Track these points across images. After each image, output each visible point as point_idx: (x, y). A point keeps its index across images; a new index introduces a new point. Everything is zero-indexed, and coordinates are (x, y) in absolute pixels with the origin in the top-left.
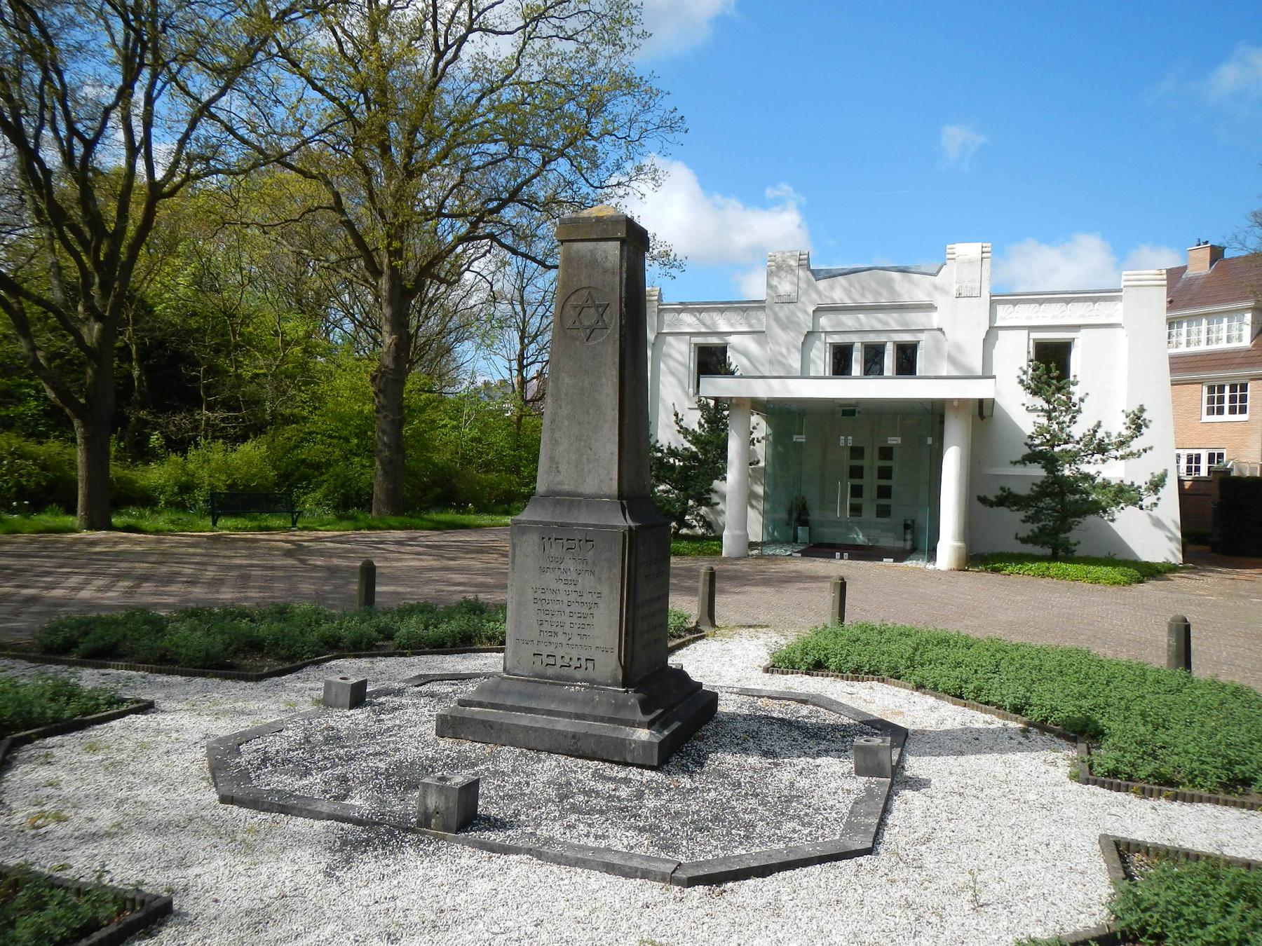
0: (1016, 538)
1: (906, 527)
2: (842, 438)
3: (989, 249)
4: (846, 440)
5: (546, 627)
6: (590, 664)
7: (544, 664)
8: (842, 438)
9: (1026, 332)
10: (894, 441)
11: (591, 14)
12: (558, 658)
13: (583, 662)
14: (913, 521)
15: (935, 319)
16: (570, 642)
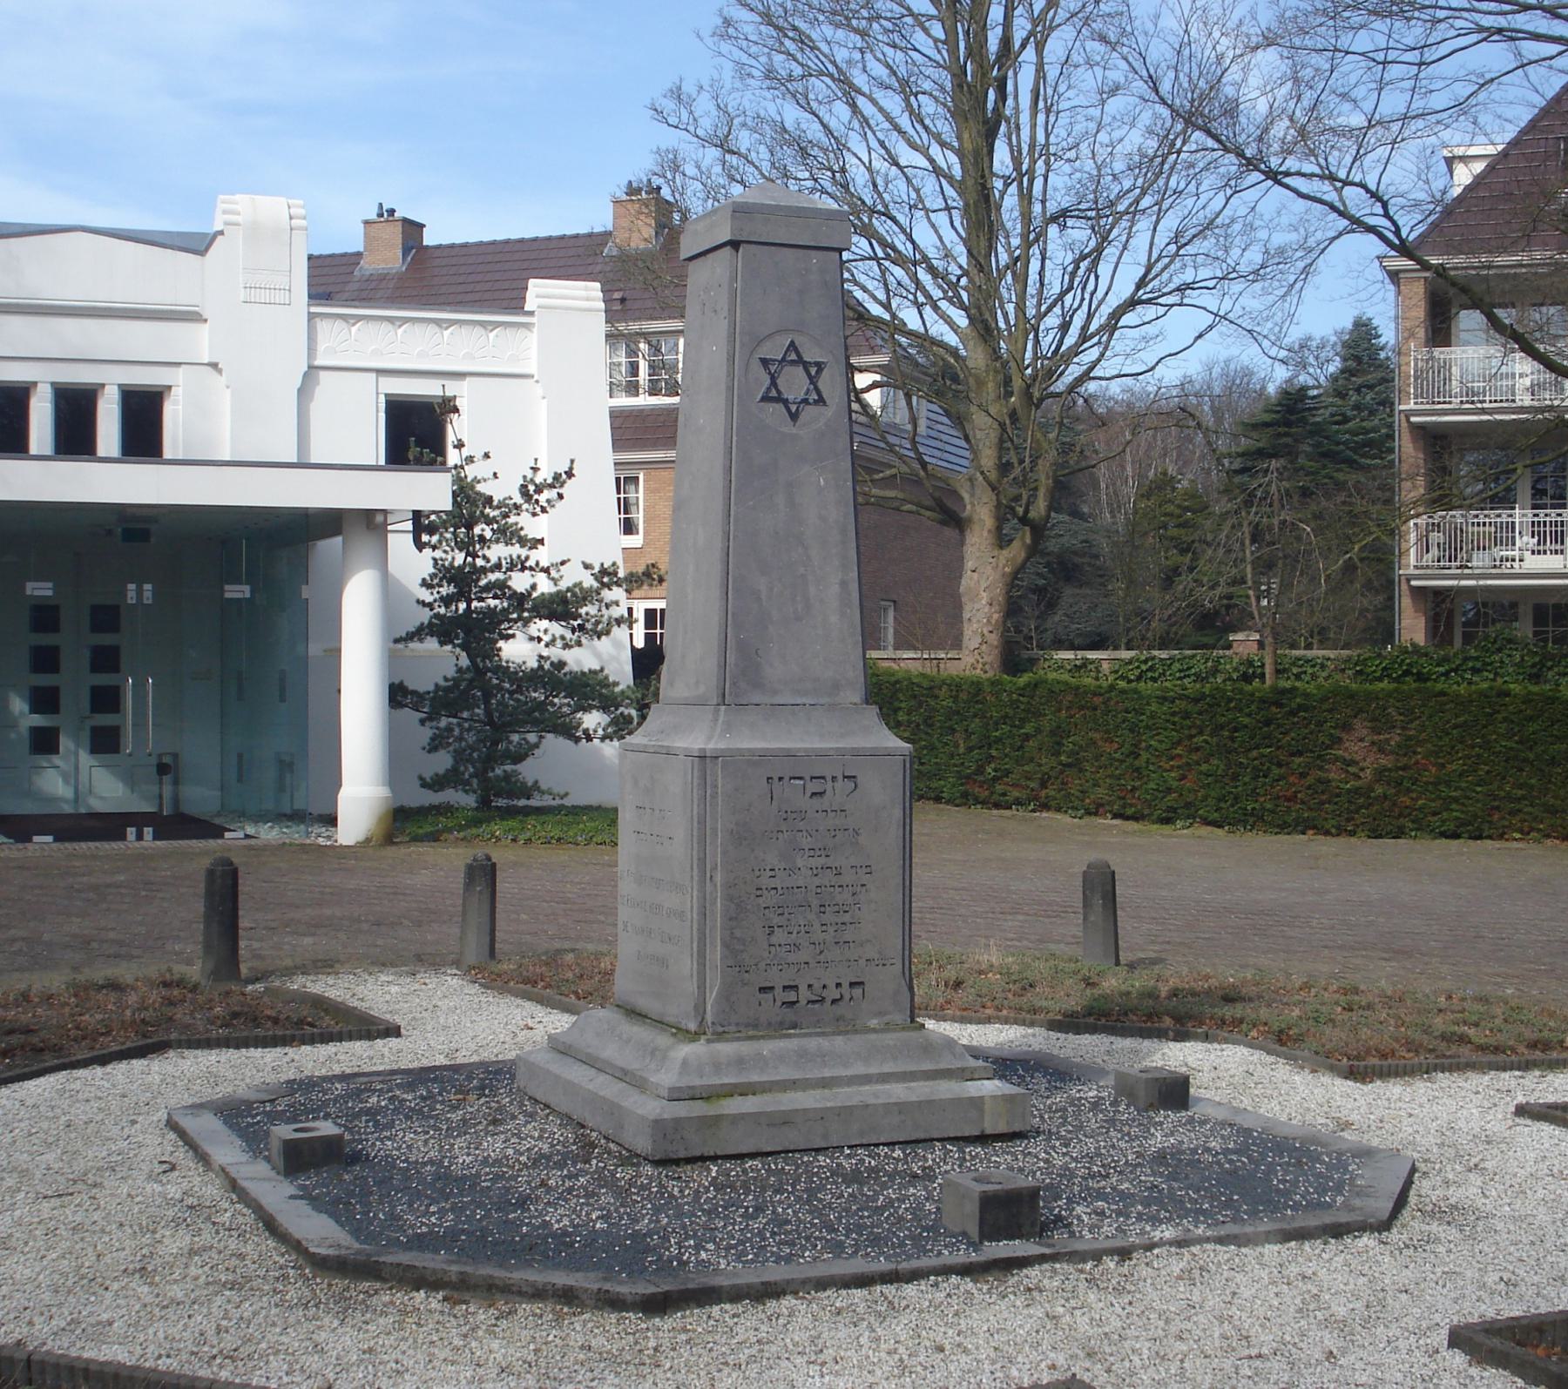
0: (423, 786)
1: (162, 769)
2: (132, 587)
3: (302, 212)
4: (140, 592)
5: (779, 937)
6: (857, 992)
7: (779, 1003)
8: (132, 587)
9: (374, 375)
10: (41, 589)
11: (851, 45)
12: (803, 989)
13: (845, 988)
14: (175, 756)
15: (199, 342)
16: (822, 958)
